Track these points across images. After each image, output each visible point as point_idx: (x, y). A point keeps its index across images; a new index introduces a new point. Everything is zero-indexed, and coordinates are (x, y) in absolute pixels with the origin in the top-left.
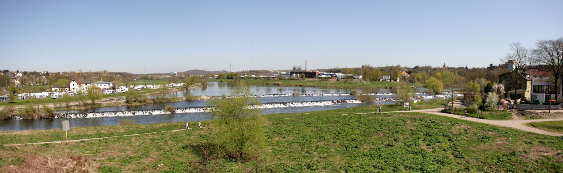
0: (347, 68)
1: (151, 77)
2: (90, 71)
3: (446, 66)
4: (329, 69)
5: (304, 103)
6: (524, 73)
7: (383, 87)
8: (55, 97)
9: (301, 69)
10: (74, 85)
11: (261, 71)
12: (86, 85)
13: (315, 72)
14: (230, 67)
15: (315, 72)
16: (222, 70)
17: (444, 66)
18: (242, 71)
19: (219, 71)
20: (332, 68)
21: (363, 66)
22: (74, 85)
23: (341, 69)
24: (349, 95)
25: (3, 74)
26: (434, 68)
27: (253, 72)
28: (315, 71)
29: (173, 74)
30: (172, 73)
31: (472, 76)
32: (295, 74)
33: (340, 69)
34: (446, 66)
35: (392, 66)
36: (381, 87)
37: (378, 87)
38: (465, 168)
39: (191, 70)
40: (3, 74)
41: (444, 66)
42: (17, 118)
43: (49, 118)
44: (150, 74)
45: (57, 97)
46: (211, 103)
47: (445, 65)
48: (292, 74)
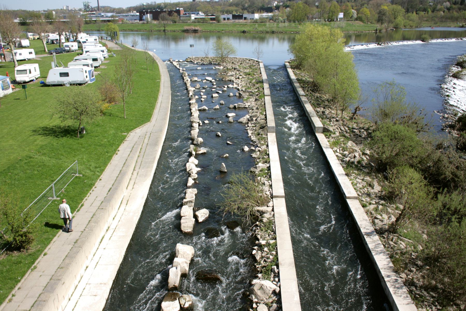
4: (139, 5)
9: (90, 7)
20: (145, 4)
23: (162, 5)
32: (149, 15)
37: (369, 31)
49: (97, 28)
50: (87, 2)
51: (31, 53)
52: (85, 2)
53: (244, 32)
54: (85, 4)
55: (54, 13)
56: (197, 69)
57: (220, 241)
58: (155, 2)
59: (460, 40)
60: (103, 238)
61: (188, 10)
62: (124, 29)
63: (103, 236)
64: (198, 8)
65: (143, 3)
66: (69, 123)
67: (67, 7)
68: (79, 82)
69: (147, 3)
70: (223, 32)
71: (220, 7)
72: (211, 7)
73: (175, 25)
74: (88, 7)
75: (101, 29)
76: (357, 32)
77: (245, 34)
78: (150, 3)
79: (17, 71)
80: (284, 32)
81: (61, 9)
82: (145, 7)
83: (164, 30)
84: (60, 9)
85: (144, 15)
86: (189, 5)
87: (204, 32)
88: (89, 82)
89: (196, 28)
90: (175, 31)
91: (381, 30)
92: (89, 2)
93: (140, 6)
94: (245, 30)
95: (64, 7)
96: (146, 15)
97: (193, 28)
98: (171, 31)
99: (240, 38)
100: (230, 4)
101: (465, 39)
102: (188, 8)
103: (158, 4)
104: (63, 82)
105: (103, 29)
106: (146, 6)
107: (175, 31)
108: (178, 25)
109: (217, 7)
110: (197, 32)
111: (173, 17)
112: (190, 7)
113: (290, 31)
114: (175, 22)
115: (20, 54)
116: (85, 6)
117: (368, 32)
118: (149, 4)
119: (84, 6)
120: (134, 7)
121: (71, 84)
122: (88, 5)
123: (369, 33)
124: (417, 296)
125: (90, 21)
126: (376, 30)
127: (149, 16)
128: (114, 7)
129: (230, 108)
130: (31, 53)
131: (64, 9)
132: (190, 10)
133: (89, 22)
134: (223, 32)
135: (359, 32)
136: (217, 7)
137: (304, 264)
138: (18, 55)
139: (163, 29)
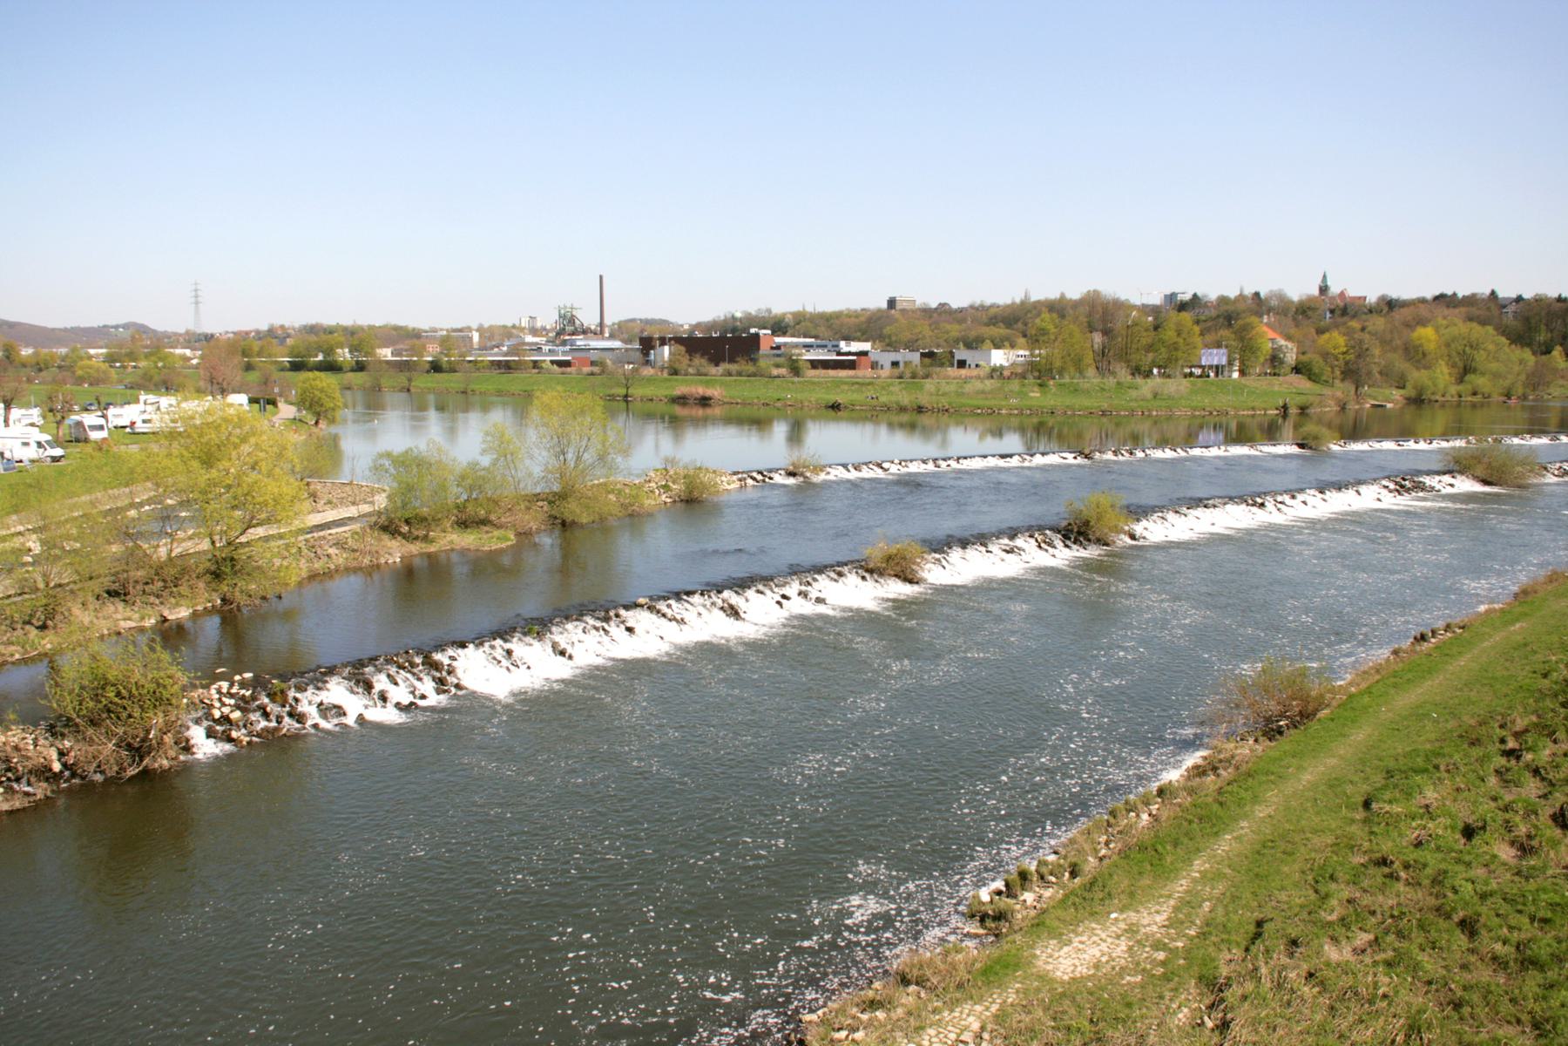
0: (1034, 298)
2: (1241, 290)
3: (1335, 289)
4: (722, 318)
5: (823, 585)
7: (1271, 409)
9: (577, 322)
11: (371, 328)
13: (757, 335)
14: (197, 303)
15: (757, 335)
17: (1324, 289)
18: (264, 327)
19: (105, 326)
20: (738, 315)
21: (892, 303)
23: (789, 318)
24: (1295, 450)
26: (414, 329)
27: (331, 333)
28: (753, 331)
31: (219, 397)
32: (666, 348)
33: (784, 314)
34: (1335, 289)
35: (1023, 303)
36: (1265, 410)
37: (1253, 409)
38: (1513, 875)
41: (1324, 289)
42: (1198, 922)
43: (948, 938)
47: (1329, 283)
50: (569, 305)
52: (565, 307)
53: (835, 407)
54: (562, 312)
55: (476, 337)
58: (769, 311)
59: (1183, 454)
61: (859, 334)
64: (888, 328)
65: (733, 311)
69: (744, 312)
70: (779, 404)
71: (957, 327)
72: (930, 325)
76: (1203, 413)
77: (839, 413)
78: (753, 313)
80: (952, 410)
82: (738, 323)
83: (626, 396)
85: (653, 348)
86: (863, 319)
87: (728, 403)
89: (709, 392)
90: (651, 400)
91: (1307, 408)
94: (840, 401)
96: (658, 349)
97: (701, 391)
98: (642, 400)
99: (828, 419)
100: (991, 319)
101: (1564, 439)
102: (860, 330)
103: (776, 316)
106: (741, 320)
107: (651, 400)
109: (948, 327)
110: (709, 406)
112: (864, 326)
113: (971, 406)
117: (1251, 413)
118: (750, 314)
119: (560, 317)
122: (573, 316)
123: (1253, 416)
124: (1053, 879)
126: (1285, 407)
132: (863, 334)
134: (779, 404)
135: (1211, 413)
136: (948, 327)
137: (769, 841)
139: (623, 391)
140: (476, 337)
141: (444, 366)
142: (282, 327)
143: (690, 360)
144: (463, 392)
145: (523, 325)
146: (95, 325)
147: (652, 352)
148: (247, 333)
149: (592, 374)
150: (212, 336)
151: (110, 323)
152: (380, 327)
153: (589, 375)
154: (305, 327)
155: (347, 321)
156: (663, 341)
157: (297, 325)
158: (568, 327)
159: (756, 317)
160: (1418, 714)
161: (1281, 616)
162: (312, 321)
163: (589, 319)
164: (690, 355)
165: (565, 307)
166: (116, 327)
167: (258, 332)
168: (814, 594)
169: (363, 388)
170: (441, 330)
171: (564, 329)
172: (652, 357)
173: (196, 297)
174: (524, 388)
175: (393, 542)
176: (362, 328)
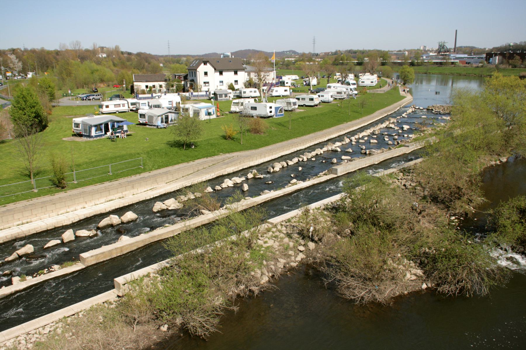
1: (187, 60)
4: (504, 45)
6: (515, 55)
8: (269, 114)
9: (445, 47)
10: (206, 74)
12: (236, 73)
14: (314, 43)
16: (288, 50)
18: (334, 51)
19: (283, 51)
20: (512, 44)
22: (206, 74)
25: (222, 57)
29: (224, 57)
30: (222, 54)
32: (497, 57)
39: (241, 51)
40: (222, 57)
44: (185, 56)
45: (272, 114)
46: (35, 117)
48: (492, 57)
49: (425, 71)
50: (443, 42)
51: (285, 91)
52: (441, 42)
54: (440, 44)
55: (407, 53)
56: (421, 117)
57: (340, 280)
60: (112, 200)
62: (453, 72)
63: (112, 198)
66: (183, 139)
67: (425, 47)
68: (263, 116)
73: (513, 70)
74: (443, 48)
75: (429, 71)
78: (518, 43)
79: (234, 103)
81: (418, 49)
82: (511, 48)
84: (416, 49)
88: (274, 117)
92: (445, 42)
93: (506, 46)
95: (421, 47)
96: (494, 58)
104: (252, 114)
105: (430, 71)
106: (512, 46)
108: (517, 70)
111: (513, 61)
114: (515, 67)
115: (277, 91)
116: (440, 46)
118: (517, 44)
119: (439, 46)
120: (498, 47)
121: (257, 117)
122: (444, 45)
125: (421, 62)
127: (497, 59)
128: (480, 47)
129: (361, 153)
130: (285, 91)
131: (421, 49)
133: (420, 64)
138: (274, 91)
140: (407, 53)
141: (415, 64)
142: (340, 51)
143: (522, 62)
144: (425, 73)
145: (421, 49)
146: (268, 52)
147: (491, 59)
148: (329, 53)
149: (478, 67)
150: (318, 54)
151: (286, 50)
152: (372, 50)
153: (476, 67)
154: (347, 51)
155: (361, 49)
156: (496, 55)
157: (344, 50)
158: (442, 50)
159: (519, 45)
160: (173, 231)
161: (491, 258)
162: (349, 49)
163: (450, 45)
164: (522, 60)
165: (441, 42)
166: (287, 52)
167: (332, 53)
168: (499, 238)
169: (251, 80)
170: (395, 51)
171: (440, 50)
172: (491, 61)
173: (314, 41)
174: (451, 72)
175: (178, 140)
176: (366, 51)
